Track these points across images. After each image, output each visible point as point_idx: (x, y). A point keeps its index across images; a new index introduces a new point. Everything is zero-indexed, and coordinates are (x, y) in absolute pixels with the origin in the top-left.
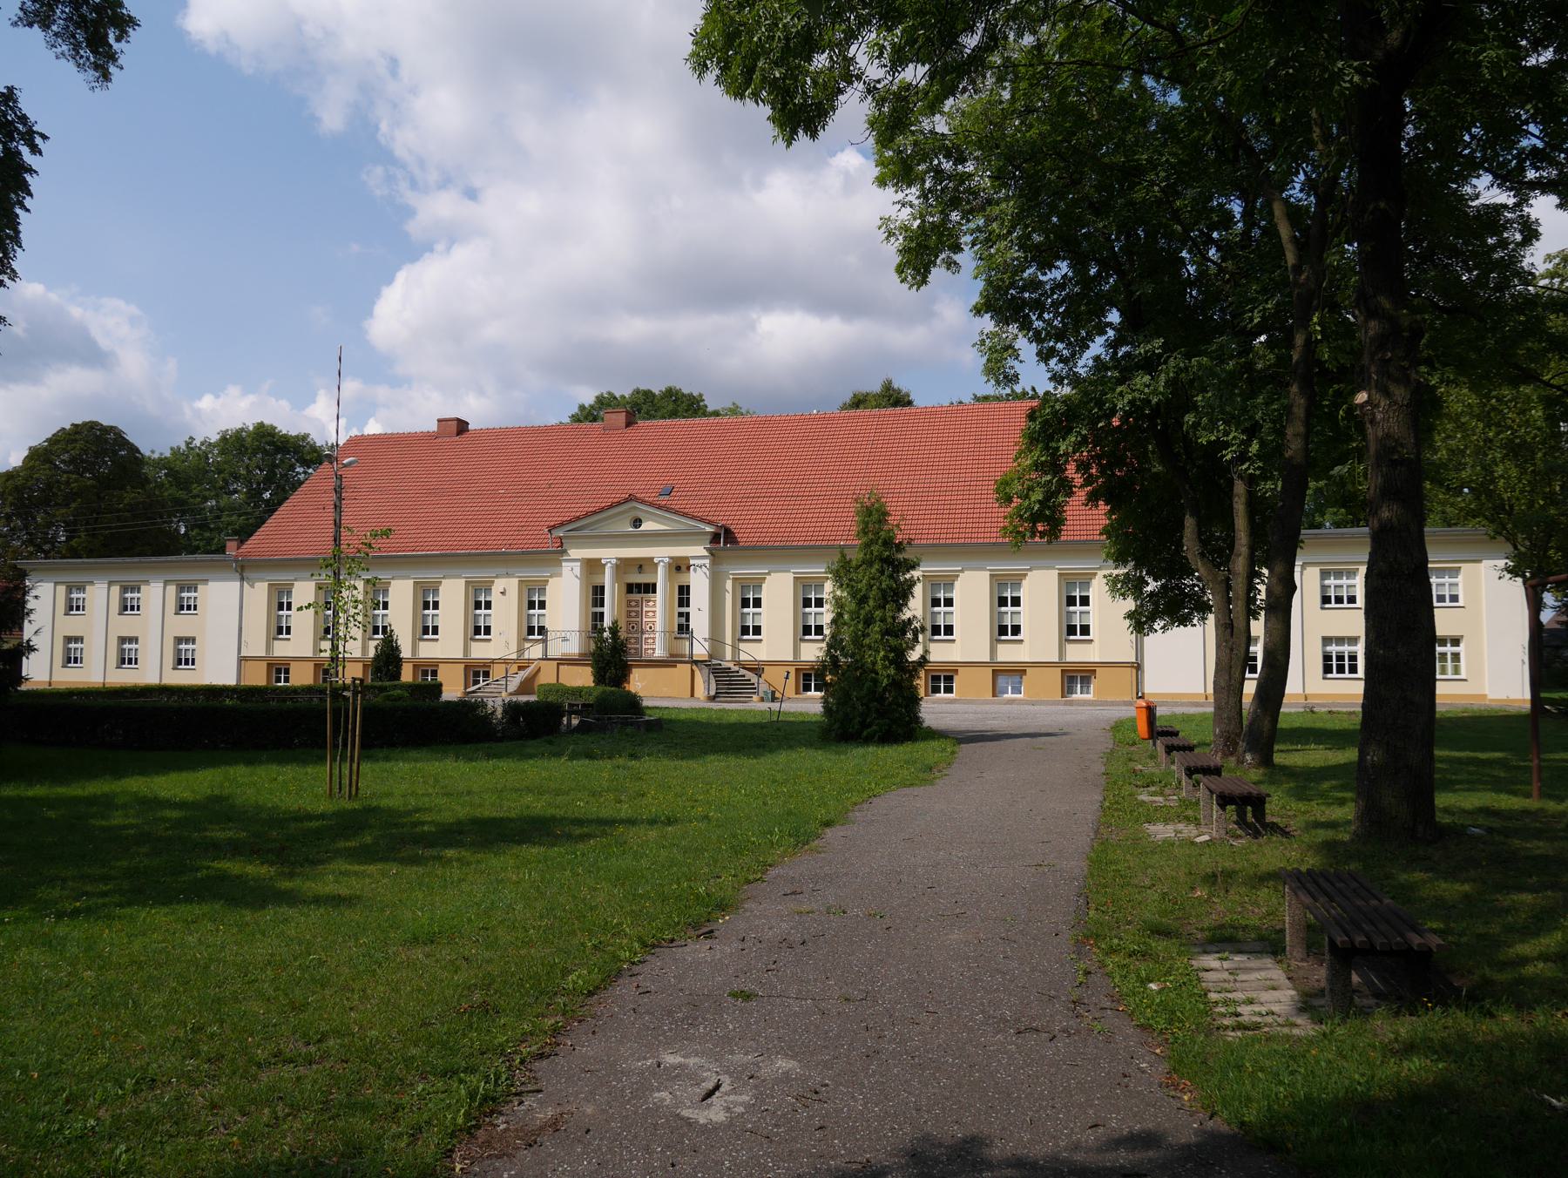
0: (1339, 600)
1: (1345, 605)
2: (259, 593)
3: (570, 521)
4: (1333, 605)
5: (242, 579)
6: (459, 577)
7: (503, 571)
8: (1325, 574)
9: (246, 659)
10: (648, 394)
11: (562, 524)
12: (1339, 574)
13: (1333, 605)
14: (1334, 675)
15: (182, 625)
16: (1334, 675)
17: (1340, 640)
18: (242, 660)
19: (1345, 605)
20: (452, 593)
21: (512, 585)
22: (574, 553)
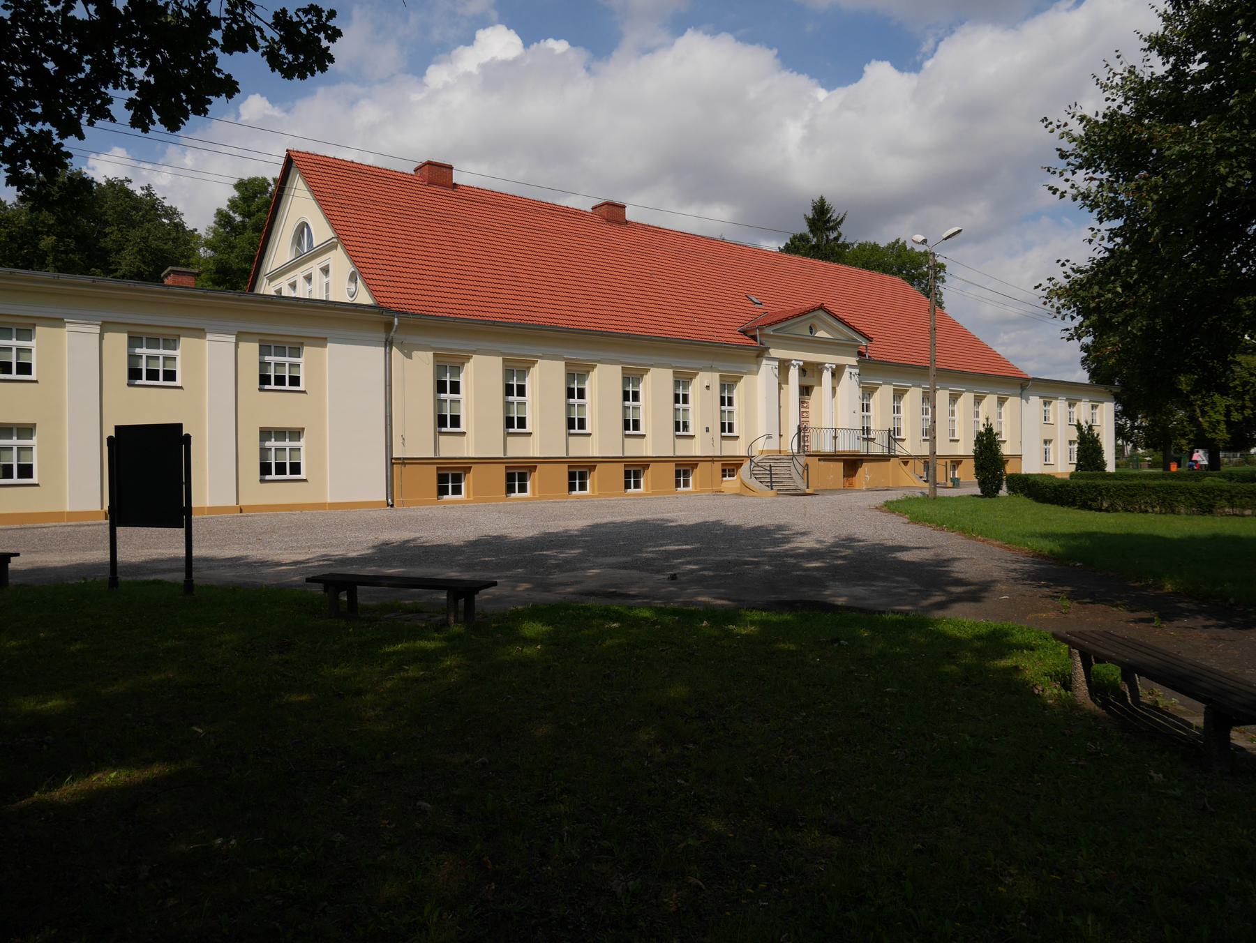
0: (280, 380)
1: (161, 382)
2: (417, 369)
3: (776, 323)
4: (144, 381)
5: (389, 344)
6: (919, 386)
7: (707, 363)
8: (134, 341)
9: (404, 461)
10: (303, 77)
11: (770, 325)
12: (153, 342)
13: (144, 381)
14: (273, 476)
15: (278, 408)
16: (273, 476)
17: (281, 434)
18: (393, 463)
19: (161, 382)
20: (545, 378)
21: (713, 379)
22: (774, 352)
